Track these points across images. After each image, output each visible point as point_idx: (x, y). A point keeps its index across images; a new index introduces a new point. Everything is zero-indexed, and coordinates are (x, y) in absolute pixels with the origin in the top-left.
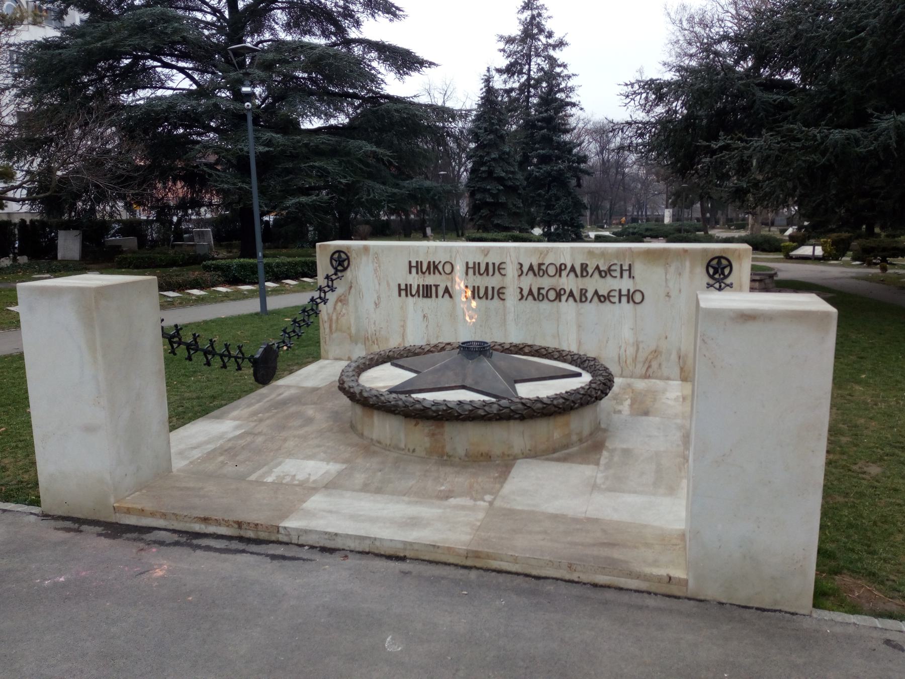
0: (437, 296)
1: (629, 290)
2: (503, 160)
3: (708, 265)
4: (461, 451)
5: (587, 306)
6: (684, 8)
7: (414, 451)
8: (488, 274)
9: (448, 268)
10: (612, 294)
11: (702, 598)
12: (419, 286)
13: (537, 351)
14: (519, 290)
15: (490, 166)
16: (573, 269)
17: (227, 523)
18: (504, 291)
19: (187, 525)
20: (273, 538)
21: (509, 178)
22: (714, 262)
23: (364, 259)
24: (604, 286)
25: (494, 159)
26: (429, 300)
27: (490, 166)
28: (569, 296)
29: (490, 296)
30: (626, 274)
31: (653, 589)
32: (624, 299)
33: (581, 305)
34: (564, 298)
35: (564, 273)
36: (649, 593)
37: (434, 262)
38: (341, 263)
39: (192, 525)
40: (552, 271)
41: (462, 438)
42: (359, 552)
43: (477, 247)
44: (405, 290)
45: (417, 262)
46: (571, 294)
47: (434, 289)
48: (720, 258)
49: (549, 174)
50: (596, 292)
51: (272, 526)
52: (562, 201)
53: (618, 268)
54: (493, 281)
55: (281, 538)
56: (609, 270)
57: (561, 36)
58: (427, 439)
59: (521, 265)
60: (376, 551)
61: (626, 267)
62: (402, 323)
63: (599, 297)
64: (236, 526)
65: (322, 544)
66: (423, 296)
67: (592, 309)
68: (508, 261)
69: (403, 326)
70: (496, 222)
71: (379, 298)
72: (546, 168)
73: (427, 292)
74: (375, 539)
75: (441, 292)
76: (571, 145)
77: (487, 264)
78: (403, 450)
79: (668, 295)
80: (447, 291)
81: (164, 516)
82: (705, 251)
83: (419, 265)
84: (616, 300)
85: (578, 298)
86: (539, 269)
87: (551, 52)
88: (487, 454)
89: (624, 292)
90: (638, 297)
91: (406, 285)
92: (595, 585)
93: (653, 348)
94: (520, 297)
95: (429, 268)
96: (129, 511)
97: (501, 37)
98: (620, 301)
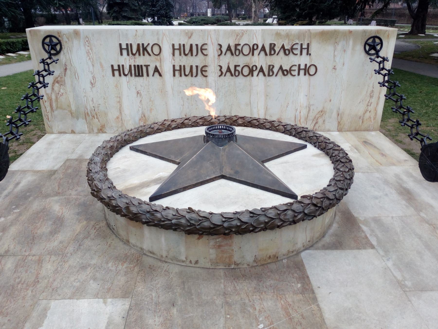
0: (148, 75)
1: (306, 65)
3: (366, 43)
5: (273, 79)
7: (197, 262)
10: (293, 68)
12: (130, 66)
13: (183, 123)
22: (47, 40)
24: (286, 61)
26: (141, 78)
28: (155, 71)
29: (194, 74)
30: (304, 52)
32: (302, 72)
33: (268, 78)
34: (255, 73)
35: (256, 52)
37: (143, 44)
38: (373, 47)
40: (246, 50)
43: (181, 30)
44: (118, 70)
48: (374, 37)
50: (281, 68)
53: (299, 47)
54: (196, 61)
56: (292, 49)
58: (212, 251)
59: (221, 46)
61: (305, 46)
62: (118, 100)
63: (283, 71)
66: (136, 76)
67: (277, 81)
68: (209, 43)
70: (123, 14)
71: (94, 78)
73: (138, 71)
75: (151, 71)
77: (191, 45)
78: (183, 262)
79: (334, 68)
80: (156, 70)
82: (365, 31)
83: (129, 47)
84: (296, 73)
85: (266, 73)
86: (236, 49)
88: (274, 256)
89: (302, 67)
93: (320, 109)
94: (220, 73)
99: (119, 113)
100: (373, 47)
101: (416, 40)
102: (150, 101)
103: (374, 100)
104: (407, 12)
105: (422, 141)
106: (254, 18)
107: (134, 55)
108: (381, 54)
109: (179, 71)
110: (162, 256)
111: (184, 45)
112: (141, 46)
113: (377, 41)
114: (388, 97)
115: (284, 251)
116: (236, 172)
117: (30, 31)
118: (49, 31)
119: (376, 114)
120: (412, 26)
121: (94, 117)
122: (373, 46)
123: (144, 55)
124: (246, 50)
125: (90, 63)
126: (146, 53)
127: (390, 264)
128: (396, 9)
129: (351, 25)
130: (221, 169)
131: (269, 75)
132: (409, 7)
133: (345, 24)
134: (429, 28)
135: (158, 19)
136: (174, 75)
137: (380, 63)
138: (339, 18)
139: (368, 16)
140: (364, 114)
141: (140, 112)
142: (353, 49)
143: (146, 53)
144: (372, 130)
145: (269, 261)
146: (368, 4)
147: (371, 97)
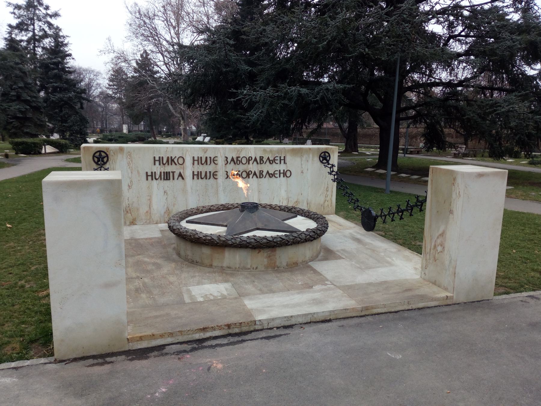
0: (173, 179)
1: (284, 170)
2: (27, 88)
3: (320, 156)
4: (284, 264)
5: (263, 180)
6: (136, 4)
7: (257, 268)
8: (207, 164)
9: (181, 161)
10: (276, 173)
11: (458, 302)
12: (161, 173)
13: (210, 209)
14: (226, 173)
15: (17, 92)
16: (256, 160)
17: (220, 328)
18: (216, 173)
19: (190, 336)
20: (252, 329)
21: (33, 101)
22: (98, 154)
23: (120, 156)
24: (272, 168)
25: (20, 87)
26: (168, 181)
27: (17, 92)
28: (179, 176)
29: (208, 177)
30: (282, 162)
31: (441, 304)
32: (282, 175)
33: (260, 179)
34: (251, 176)
35: (251, 162)
36: (440, 306)
37: (171, 157)
38: (325, 158)
39: (194, 335)
40: (244, 161)
41: (285, 256)
42: (75, 360)
43: (199, 148)
44: (151, 176)
45: (160, 157)
46: (255, 174)
47: (171, 174)
48: (325, 152)
49: (61, 100)
50: (268, 172)
51: (251, 321)
52: (73, 118)
53: (278, 158)
54: (210, 168)
55: (257, 327)
56: (274, 160)
57: (57, 10)
58: (265, 260)
59: (227, 158)
60: (314, 320)
61: (282, 158)
62: (149, 198)
63: (269, 174)
64: (226, 328)
65: (282, 325)
66: (164, 179)
67: (266, 181)
68: (219, 155)
69: (150, 200)
70: (25, 130)
71: (131, 181)
72: (59, 95)
73: (167, 176)
74: (314, 313)
75: (176, 176)
76: (75, 82)
77: (206, 158)
78: (249, 269)
79: (302, 172)
80: (180, 175)
81: (171, 334)
82: (318, 149)
83: (161, 160)
84: (278, 176)
85: (258, 176)
86: (237, 160)
87: (49, 19)
88: (296, 263)
89: (282, 171)
90: (288, 174)
91: (152, 173)
92: (419, 309)
93: (295, 200)
94: (226, 176)
95: (168, 161)
96: (141, 338)
97: (10, 4)
98: (280, 176)
99: (148, 209)
100: (325, 158)
101: (351, 157)
102: (174, 197)
103: (329, 193)
104: (339, 131)
105: (361, 210)
106: (184, 135)
107: (164, 164)
108: (330, 162)
109: (197, 175)
110: (236, 268)
111: (201, 157)
112: (170, 158)
113: (327, 154)
114: (338, 189)
115: (300, 260)
116: (266, 225)
117: (84, 148)
118: (100, 147)
119: (331, 203)
120: (346, 145)
121: (128, 212)
122: (324, 158)
123: (171, 164)
124: (244, 161)
125: (130, 172)
126: (173, 163)
127: (353, 263)
128: (329, 129)
129: (286, 144)
130: (256, 224)
131: (260, 177)
132: (341, 127)
133: (281, 143)
134: (361, 147)
135: (69, 136)
136: (193, 178)
137: (330, 168)
138: (274, 138)
139: (305, 136)
140: (324, 203)
141: (166, 207)
142: (312, 160)
143: (173, 163)
144: (331, 214)
145: (294, 265)
146: (305, 125)
147: (327, 191)
